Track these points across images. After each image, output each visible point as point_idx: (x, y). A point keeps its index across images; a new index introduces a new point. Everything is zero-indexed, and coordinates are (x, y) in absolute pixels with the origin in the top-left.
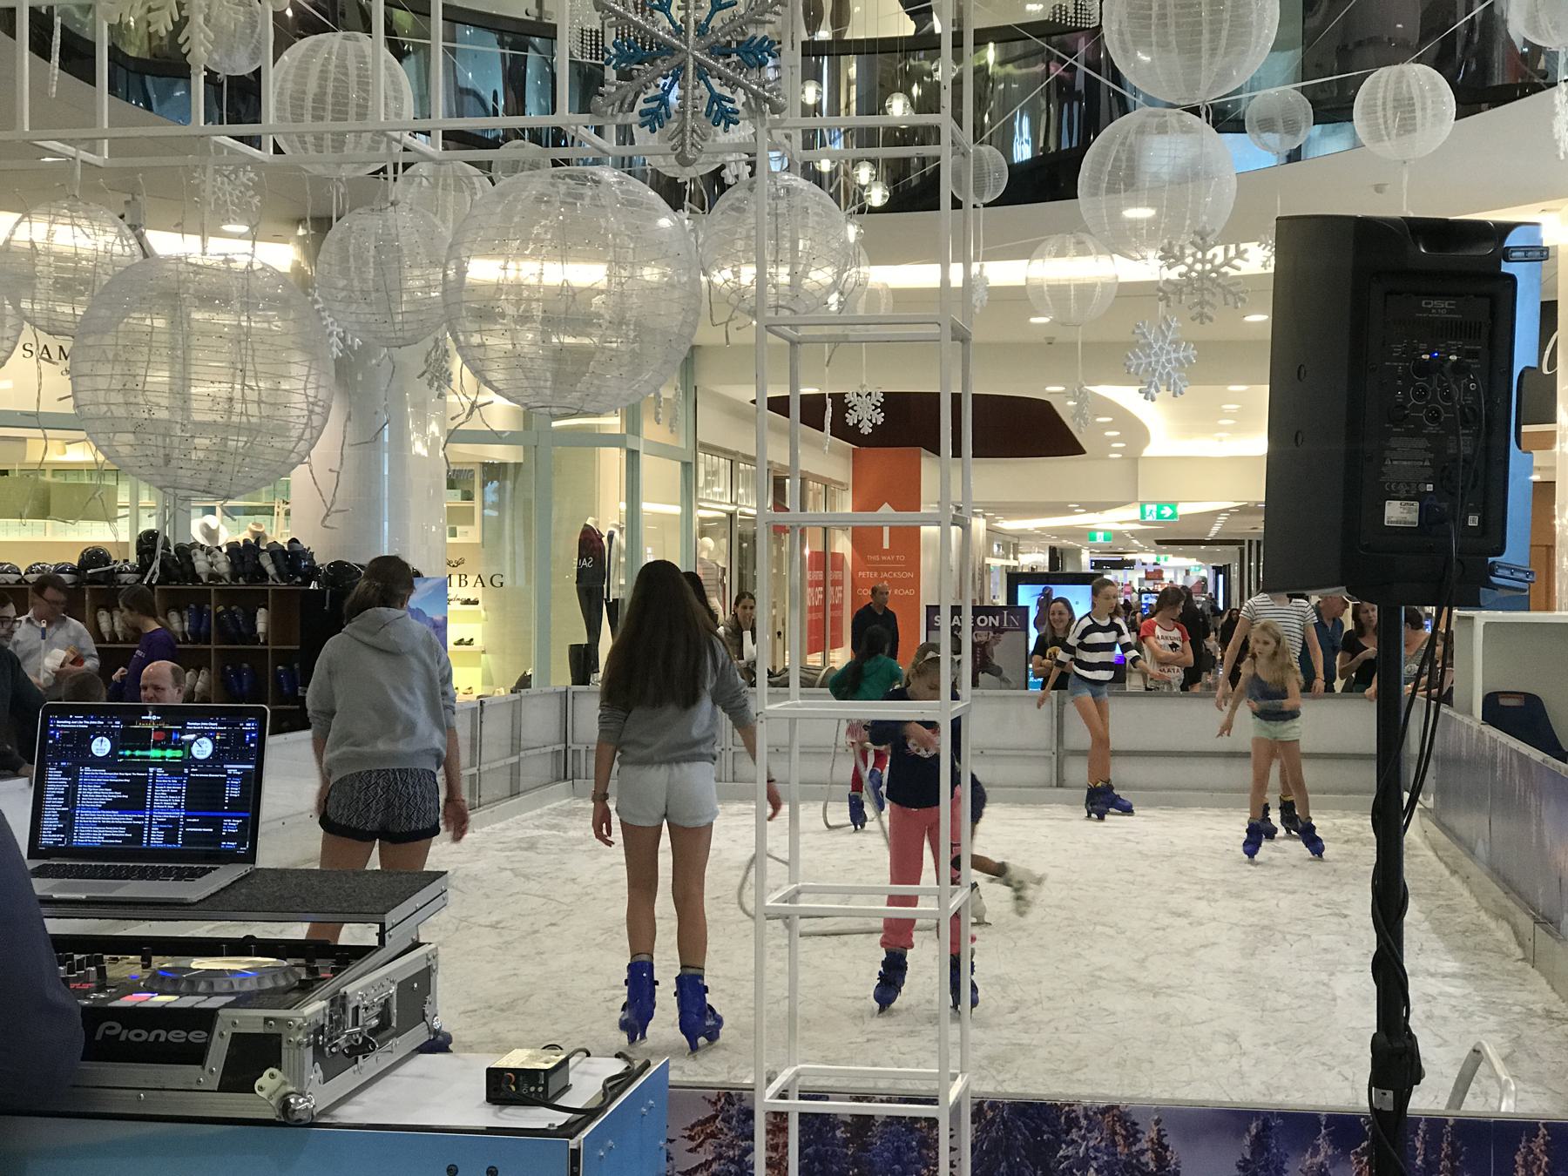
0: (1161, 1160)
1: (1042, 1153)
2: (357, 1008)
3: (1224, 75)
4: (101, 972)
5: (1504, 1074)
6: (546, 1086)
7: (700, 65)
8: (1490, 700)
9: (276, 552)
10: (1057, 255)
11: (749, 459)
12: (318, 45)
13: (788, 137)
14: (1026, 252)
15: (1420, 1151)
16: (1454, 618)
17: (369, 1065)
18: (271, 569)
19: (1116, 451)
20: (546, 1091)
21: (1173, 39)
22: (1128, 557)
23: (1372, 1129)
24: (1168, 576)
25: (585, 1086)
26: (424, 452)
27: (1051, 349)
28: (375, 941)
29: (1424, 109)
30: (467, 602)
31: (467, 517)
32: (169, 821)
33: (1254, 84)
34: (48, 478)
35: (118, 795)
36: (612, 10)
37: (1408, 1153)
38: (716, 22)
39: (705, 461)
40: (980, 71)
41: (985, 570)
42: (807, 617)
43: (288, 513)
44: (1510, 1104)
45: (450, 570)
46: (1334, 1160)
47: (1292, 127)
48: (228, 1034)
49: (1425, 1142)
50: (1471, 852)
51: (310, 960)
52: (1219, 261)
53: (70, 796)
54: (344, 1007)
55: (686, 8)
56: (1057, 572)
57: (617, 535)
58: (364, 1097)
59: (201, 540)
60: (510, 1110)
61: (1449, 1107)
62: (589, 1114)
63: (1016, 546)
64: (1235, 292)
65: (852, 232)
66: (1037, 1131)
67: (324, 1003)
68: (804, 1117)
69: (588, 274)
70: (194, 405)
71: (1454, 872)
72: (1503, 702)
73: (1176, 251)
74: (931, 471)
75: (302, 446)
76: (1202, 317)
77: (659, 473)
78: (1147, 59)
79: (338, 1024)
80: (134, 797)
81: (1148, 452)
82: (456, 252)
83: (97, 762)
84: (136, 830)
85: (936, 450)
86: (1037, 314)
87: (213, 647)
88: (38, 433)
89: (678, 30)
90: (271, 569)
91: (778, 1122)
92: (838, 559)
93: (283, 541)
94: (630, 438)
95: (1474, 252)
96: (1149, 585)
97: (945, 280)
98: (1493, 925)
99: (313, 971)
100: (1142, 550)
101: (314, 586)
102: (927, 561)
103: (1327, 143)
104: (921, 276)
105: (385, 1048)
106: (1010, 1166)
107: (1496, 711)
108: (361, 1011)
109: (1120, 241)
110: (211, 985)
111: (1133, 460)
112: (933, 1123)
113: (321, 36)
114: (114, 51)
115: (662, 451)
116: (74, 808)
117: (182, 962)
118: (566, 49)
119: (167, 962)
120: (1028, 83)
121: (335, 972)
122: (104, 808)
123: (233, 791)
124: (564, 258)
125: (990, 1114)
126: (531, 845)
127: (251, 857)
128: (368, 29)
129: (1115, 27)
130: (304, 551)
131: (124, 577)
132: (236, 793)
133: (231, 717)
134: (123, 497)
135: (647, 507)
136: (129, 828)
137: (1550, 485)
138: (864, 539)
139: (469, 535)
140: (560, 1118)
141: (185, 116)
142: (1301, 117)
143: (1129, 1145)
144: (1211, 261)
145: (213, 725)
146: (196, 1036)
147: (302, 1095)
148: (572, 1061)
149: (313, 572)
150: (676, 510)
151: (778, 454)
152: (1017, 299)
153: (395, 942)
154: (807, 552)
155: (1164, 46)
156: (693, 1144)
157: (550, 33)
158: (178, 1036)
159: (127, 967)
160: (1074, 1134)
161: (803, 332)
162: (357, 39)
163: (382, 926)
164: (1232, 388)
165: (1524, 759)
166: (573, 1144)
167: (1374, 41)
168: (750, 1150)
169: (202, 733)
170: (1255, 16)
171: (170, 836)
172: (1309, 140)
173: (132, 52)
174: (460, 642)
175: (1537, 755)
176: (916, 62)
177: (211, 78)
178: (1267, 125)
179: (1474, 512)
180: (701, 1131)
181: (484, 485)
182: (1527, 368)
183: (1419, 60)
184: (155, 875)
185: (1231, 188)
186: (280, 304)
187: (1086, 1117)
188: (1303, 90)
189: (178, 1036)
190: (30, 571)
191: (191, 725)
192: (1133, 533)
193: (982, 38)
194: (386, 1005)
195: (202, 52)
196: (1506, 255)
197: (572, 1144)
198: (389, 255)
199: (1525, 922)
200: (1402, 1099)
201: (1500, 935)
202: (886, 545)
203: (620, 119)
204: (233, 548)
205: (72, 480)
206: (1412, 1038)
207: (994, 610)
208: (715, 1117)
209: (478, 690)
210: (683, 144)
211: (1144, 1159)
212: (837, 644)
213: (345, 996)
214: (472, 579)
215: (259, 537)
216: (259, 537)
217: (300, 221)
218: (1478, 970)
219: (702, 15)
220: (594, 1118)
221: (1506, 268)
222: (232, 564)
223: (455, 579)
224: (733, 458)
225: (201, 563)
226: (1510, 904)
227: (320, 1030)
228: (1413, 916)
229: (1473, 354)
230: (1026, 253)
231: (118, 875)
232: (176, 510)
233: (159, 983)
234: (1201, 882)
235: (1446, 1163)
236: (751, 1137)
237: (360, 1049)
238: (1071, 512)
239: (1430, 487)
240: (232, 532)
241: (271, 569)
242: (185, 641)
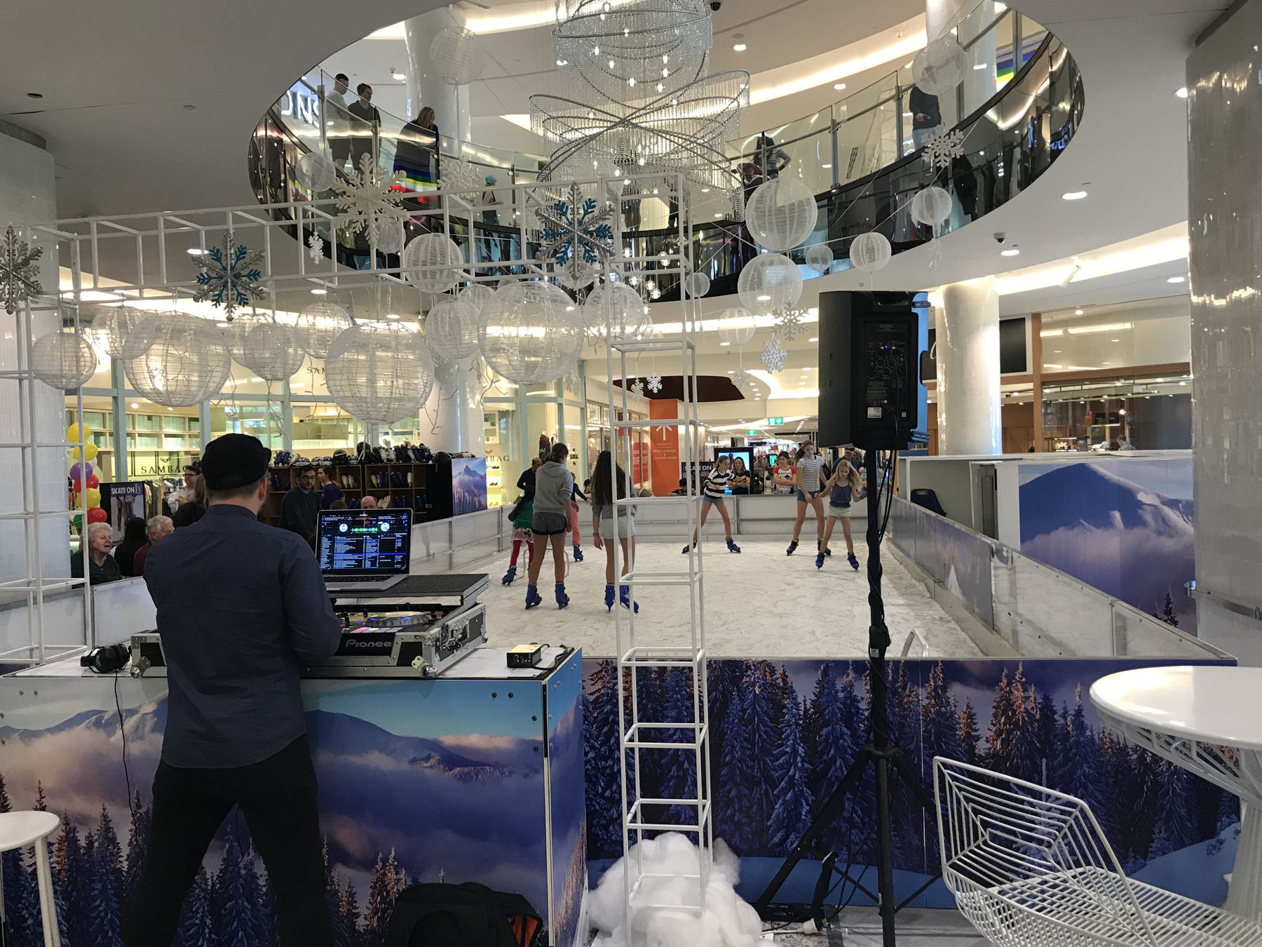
0: (785, 681)
1: (736, 681)
2: (452, 631)
3: (797, 239)
4: (347, 619)
5: (924, 642)
6: (531, 659)
7: (580, 237)
8: (914, 493)
9: (414, 449)
10: (730, 317)
11: (607, 406)
12: (422, 239)
13: (618, 266)
14: (717, 316)
15: (891, 674)
16: (898, 460)
17: (458, 654)
18: (413, 457)
19: (758, 397)
20: (531, 662)
21: (774, 220)
22: (763, 441)
23: (871, 666)
24: (780, 448)
25: (547, 660)
26: (474, 407)
27: (729, 357)
28: (459, 604)
29: (878, 250)
30: (494, 468)
31: (493, 433)
32: (372, 557)
33: (808, 242)
34: (320, 422)
35: (351, 547)
36: (543, 216)
37: (885, 674)
38: (586, 219)
39: (590, 407)
40: (697, 243)
41: (705, 448)
42: (634, 469)
43: (419, 434)
44: (927, 654)
45: (487, 455)
46: (856, 679)
47: (825, 261)
48: (400, 643)
49: (892, 670)
50: (908, 555)
51: (433, 612)
52: (796, 315)
53: (332, 549)
54: (447, 630)
55: (574, 214)
56: (734, 448)
57: (555, 438)
58: (457, 667)
59: (384, 446)
60: (517, 670)
61: (902, 656)
62: (550, 670)
63: (717, 438)
64: (805, 328)
65: (646, 310)
66: (734, 672)
67: (439, 629)
68: (638, 668)
69: (539, 332)
70: (378, 390)
71: (901, 563)
72: (919, 493)
73: (779, 311)
74: (681, 407)
75: (422, 400)
76: (790, 338)
77: (571, 413)
78: (764, 235)
79: (445, 637)
80: (358, 548)
81: (770, 398)
82: (481, 323)
83: (342, 534)
84: (359, 562)
85: (682, 399)
86: (724, 342)
87: (390, 489)
88: (314, 404)
89: (571, 223)
90: (412, 456)
91: (628, 670)
92: (645, 445)
93: (417, 445)
94: (559, 399)
95: (901, 304)
96: (773, 452)
97: (684, 329)
98: (918, 584)
99: (434, 616)
100: (769, 438)
101: (430, 462)
102: (681, 445)
103: (840, 267)
104: (674, 328)
105: (465, 647)
106: (723, 687)
107: (916, 497)
108: (455, 632)
109: (756, 310)
110: (393, 623)
111: (764, 400)
112: (691, 669)
113: (423, 236)
114: (339, 246)
115: (572, 403)
116: (334, 553)
117: (381, 614)
118: (524, 239)
119: (375, 615)
120: (716, 247)
121: (443, 616)
122: (346, 553)
123: (399, 544)
124: (528, 325)
125: (714, 666)
126: (559, 627)
127: (407, 571)
128: (443, 232)
129: (750, 220)
130: (426, 449)
131: (352, 462)
132: (400, 545)
133: (397, 514)
134: (351, 429)
135: (567, 427)
136: (356, 561)
137: (936, 404)
138: (655, 436)
139: (495, 440)
140: (538, 672)
141: (369, 267)
142: (828, 257)
143: (772, 676)
144: (794, 315)
145: (389, 517)
146: (387, 644)
147: (431, 666)
148: (542, 650)
149: (430, 457)
150: (579, 428)
151: (618, 403)
152: (715, 336)
153: (467, 603)
154: (633, 443)
155: (771, 230)
156: (593, 682)
157: (518, 231)
158: (379, 644)
159: (358, 618)
160: (749, 673)
161: (626, 347)
162: (439, 236)
163: (462, 597)
164: (805, 369)
165: (927, 515)
166: (543, 682)
167: (858, 225)
168: (617, 684)
169: (385, 521)
170: (807, 214)
171: (373, 564)
172: (832, 265)
173: (348, 246)
174: (492, 484)
175: (933, 514)
176: (671, 240)
177: (379, 254)
178: (815, 260)
179: (904, 411)
180: (596, 677)
181: (500, 420)
182: (924, 351)
183: (875, 231)
184: (367, 580)
185: (801, 286)
186: (411, 347)
187: (754, 665)
188: (829, 245)
189: (379, 644)
190: (313, 460)
191: (380, 518)
192: (765, 431)
193: (697, 229)
194: (465, 629)
195: (375, 242)
196: (914, 305)
197: (543, 683)
198: (455, 324)
199: (931, 582)
200: (883, 652)
201: (921, 588)
202: (664, 439)
203: (548, 261)
204: (397, 448)
205: (329, 423)
206: (886, 627)
207: (709, 463)
208: (601, 671)
209: (500, 504)
210: (574, 271)
211: (778, 681)
212: (646, 479)
213: (447, 626)
214: (496, 458)
215: (407, 444)
216: (407, 444)
217: (419, 313)
218: (911, 602)
219: (580, 217)
220: (552, 672)
221: (914, 310)
222: (396, 455)
223: (489, 458)
224: (601, 405)
225: (384, 455)
226: (924, 576)
227: (438, 640)
228: (884, 580)
229: (902, 346)
230: (717, 316)
231: (352, 580)
232: (372, 431)
233: (370, 623)
234: (798, 571)
235: (901, 678)
236: (617, 678)
237: (454, 647)
238: (740, 423)
239: (886, 402)
240: (396, 442)
241: (413, 457)
242: (378, 487)
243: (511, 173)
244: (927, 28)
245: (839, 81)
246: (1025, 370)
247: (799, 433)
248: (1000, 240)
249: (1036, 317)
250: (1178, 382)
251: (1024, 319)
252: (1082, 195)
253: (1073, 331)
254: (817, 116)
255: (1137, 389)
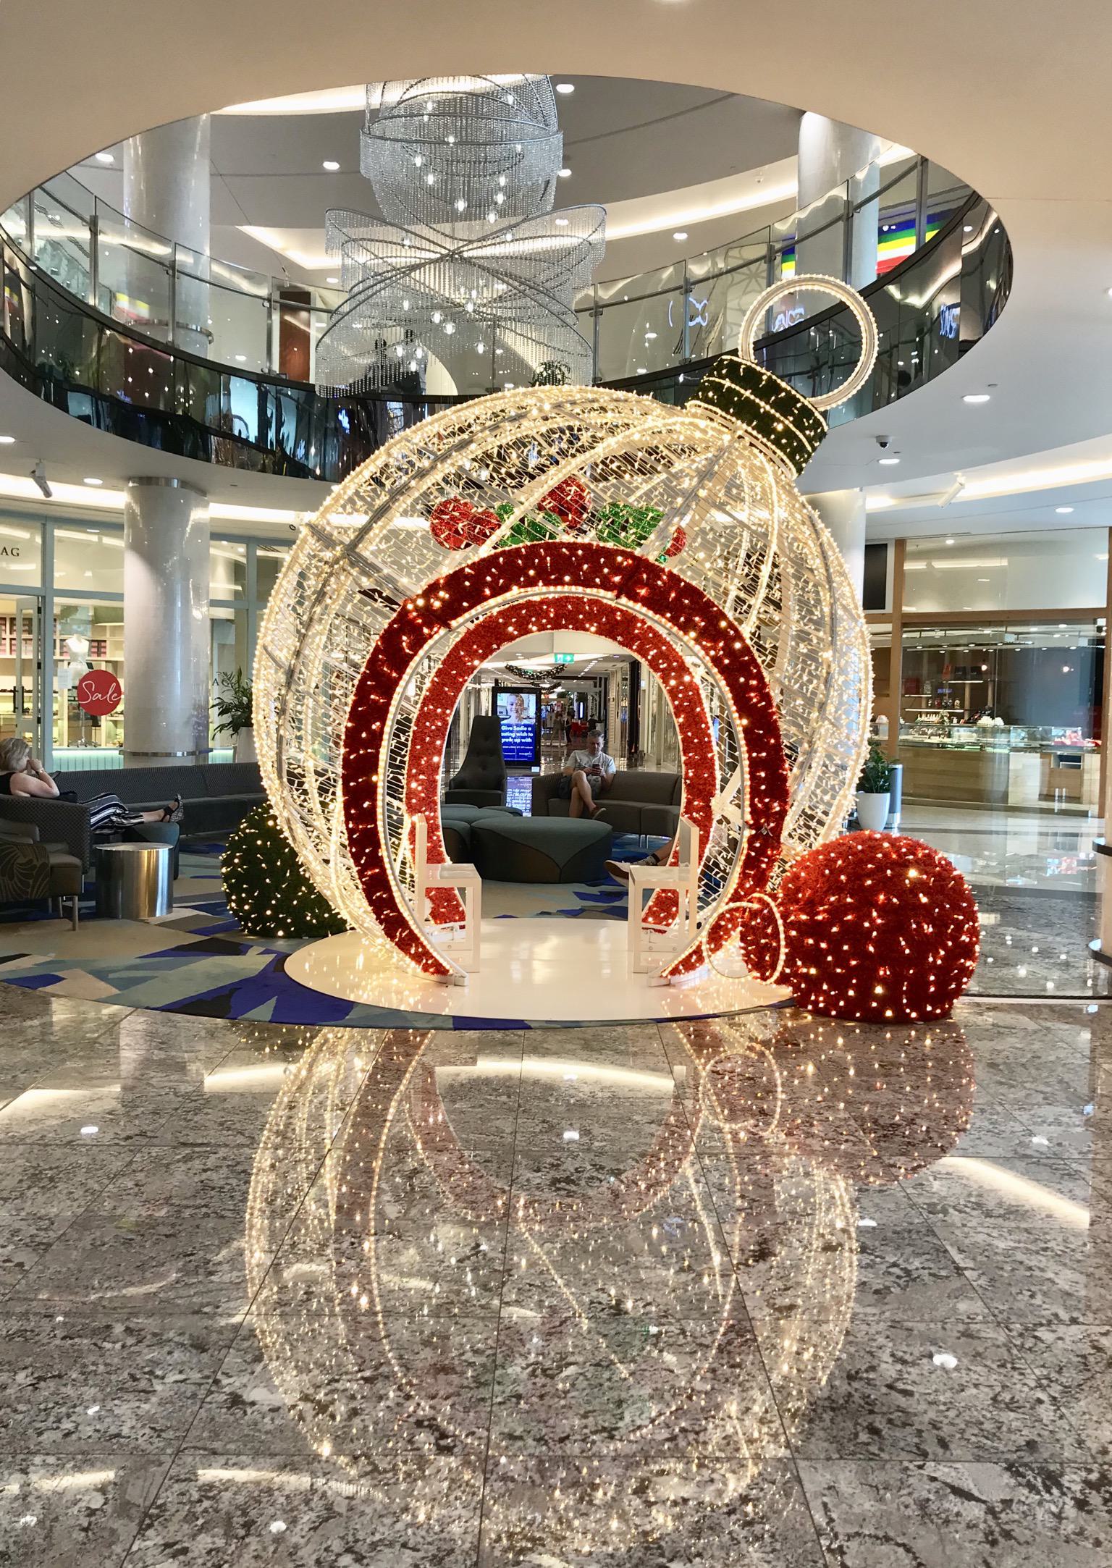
243: (267, 304)
244: (800, 182)
245: (681, 229)
246: (884, 608)
247: (583, 678)
248: (883, 445)
249: (900, 543)
250: (1051, 633)
251: (886, 546)
252: (984, 398)
253: (940, 565)
254: (671, 269)
255: (1010, 638)
